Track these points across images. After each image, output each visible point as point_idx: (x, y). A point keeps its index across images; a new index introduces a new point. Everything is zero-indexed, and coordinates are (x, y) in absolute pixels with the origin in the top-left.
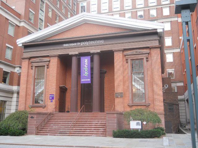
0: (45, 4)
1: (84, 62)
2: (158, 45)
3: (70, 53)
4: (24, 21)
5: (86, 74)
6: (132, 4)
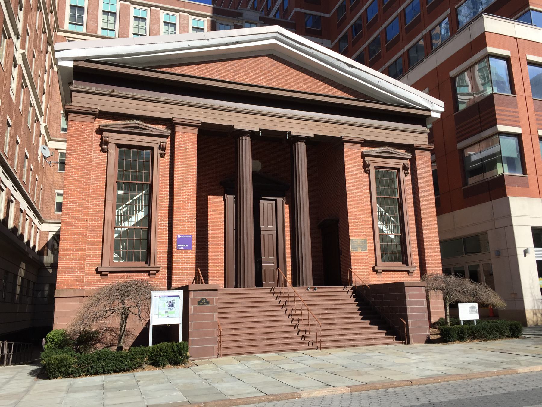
2: (427, 143)
3: (237, 126)
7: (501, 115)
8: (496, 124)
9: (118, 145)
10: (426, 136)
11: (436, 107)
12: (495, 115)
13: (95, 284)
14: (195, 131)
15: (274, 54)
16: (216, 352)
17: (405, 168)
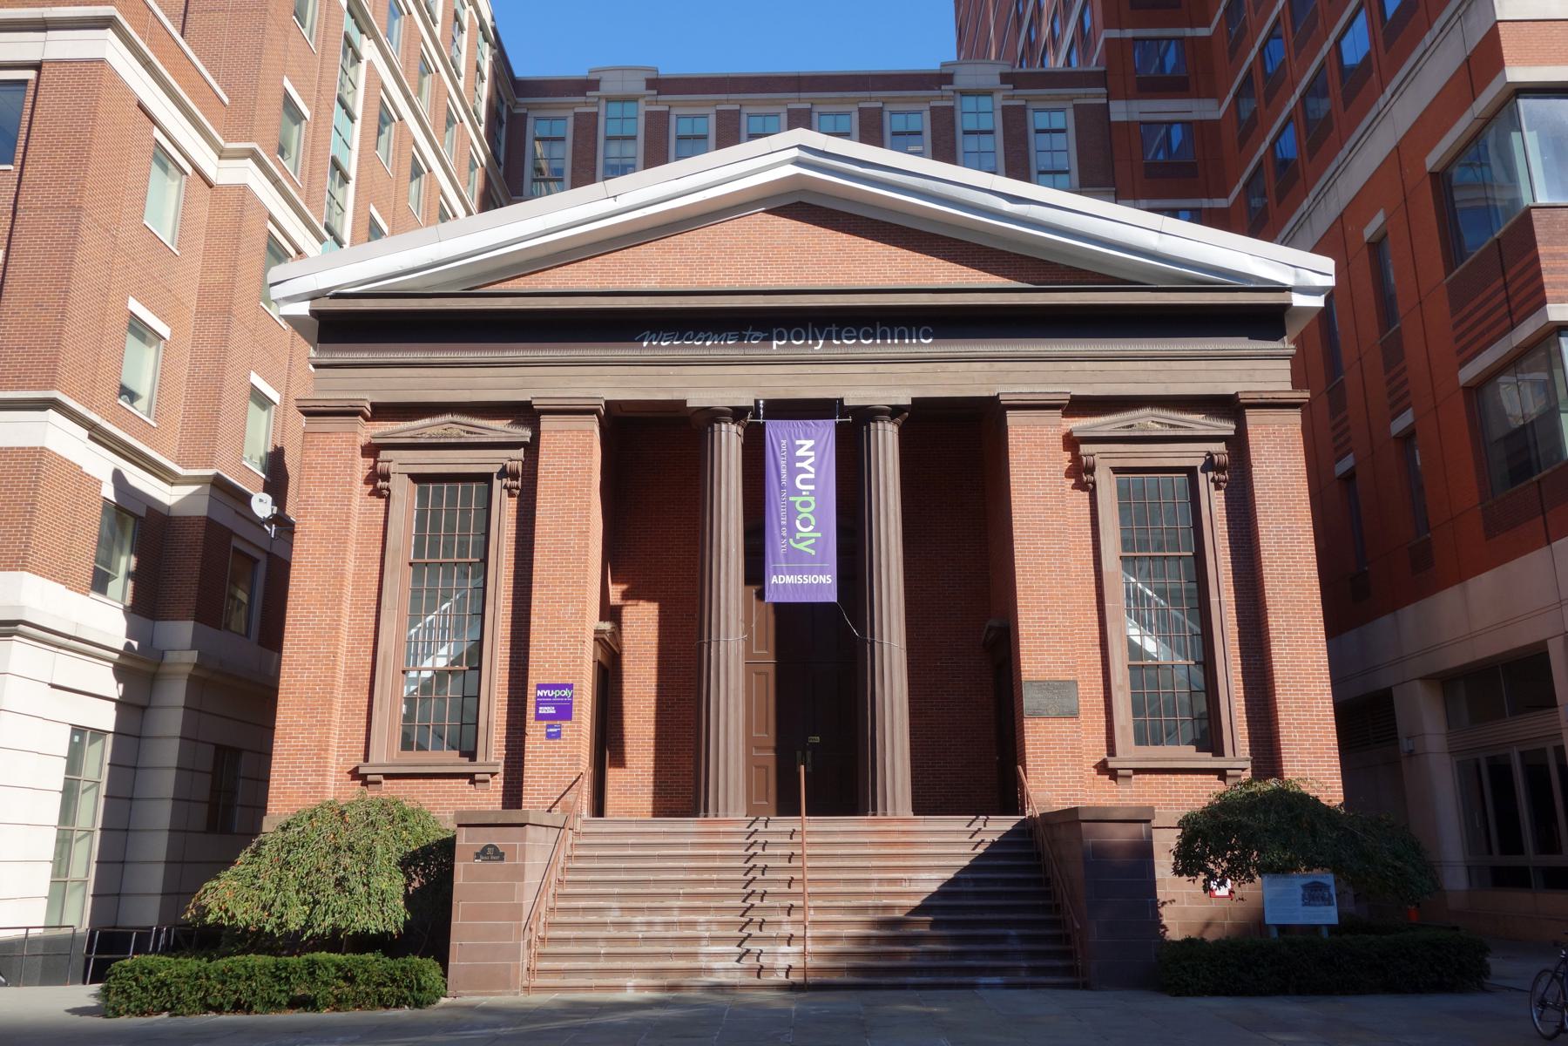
0: (363, 66)
1: (792, 459)
3: (696, 400)
5: (803, 539)
6: (1026, 144)
8: (1544, 302)
9: (416, 478)
10: (1287, 365)
12: (1539, 273)
14: (592, 426)
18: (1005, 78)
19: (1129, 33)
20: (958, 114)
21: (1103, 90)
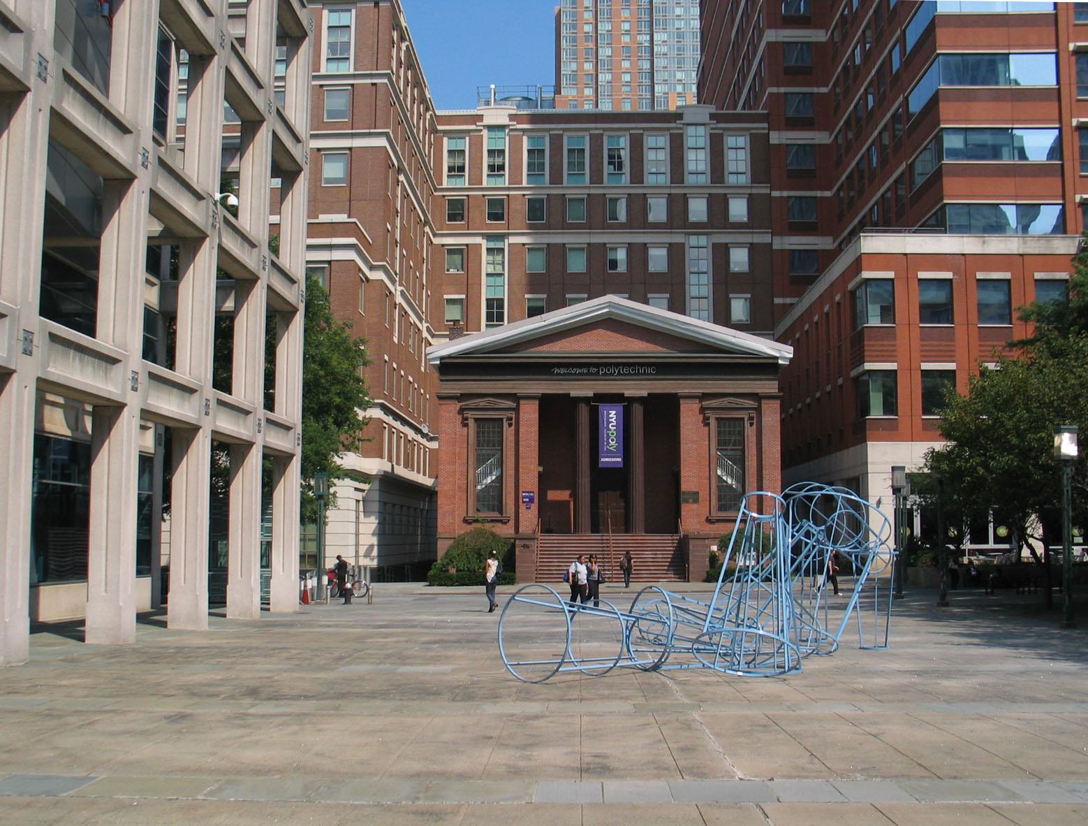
1: (608, 418)
2: (777, 391)
3: (574, 393)
4: (355, 223)
7: (871, 351)
11: (784, 353)
13: (461, 530)
15: (610, 323)
16: (534, 578)
17: (751, 418)
18: (712, 116)
19: (782, 90)
20: (685, 137)
21: (766, 125)
